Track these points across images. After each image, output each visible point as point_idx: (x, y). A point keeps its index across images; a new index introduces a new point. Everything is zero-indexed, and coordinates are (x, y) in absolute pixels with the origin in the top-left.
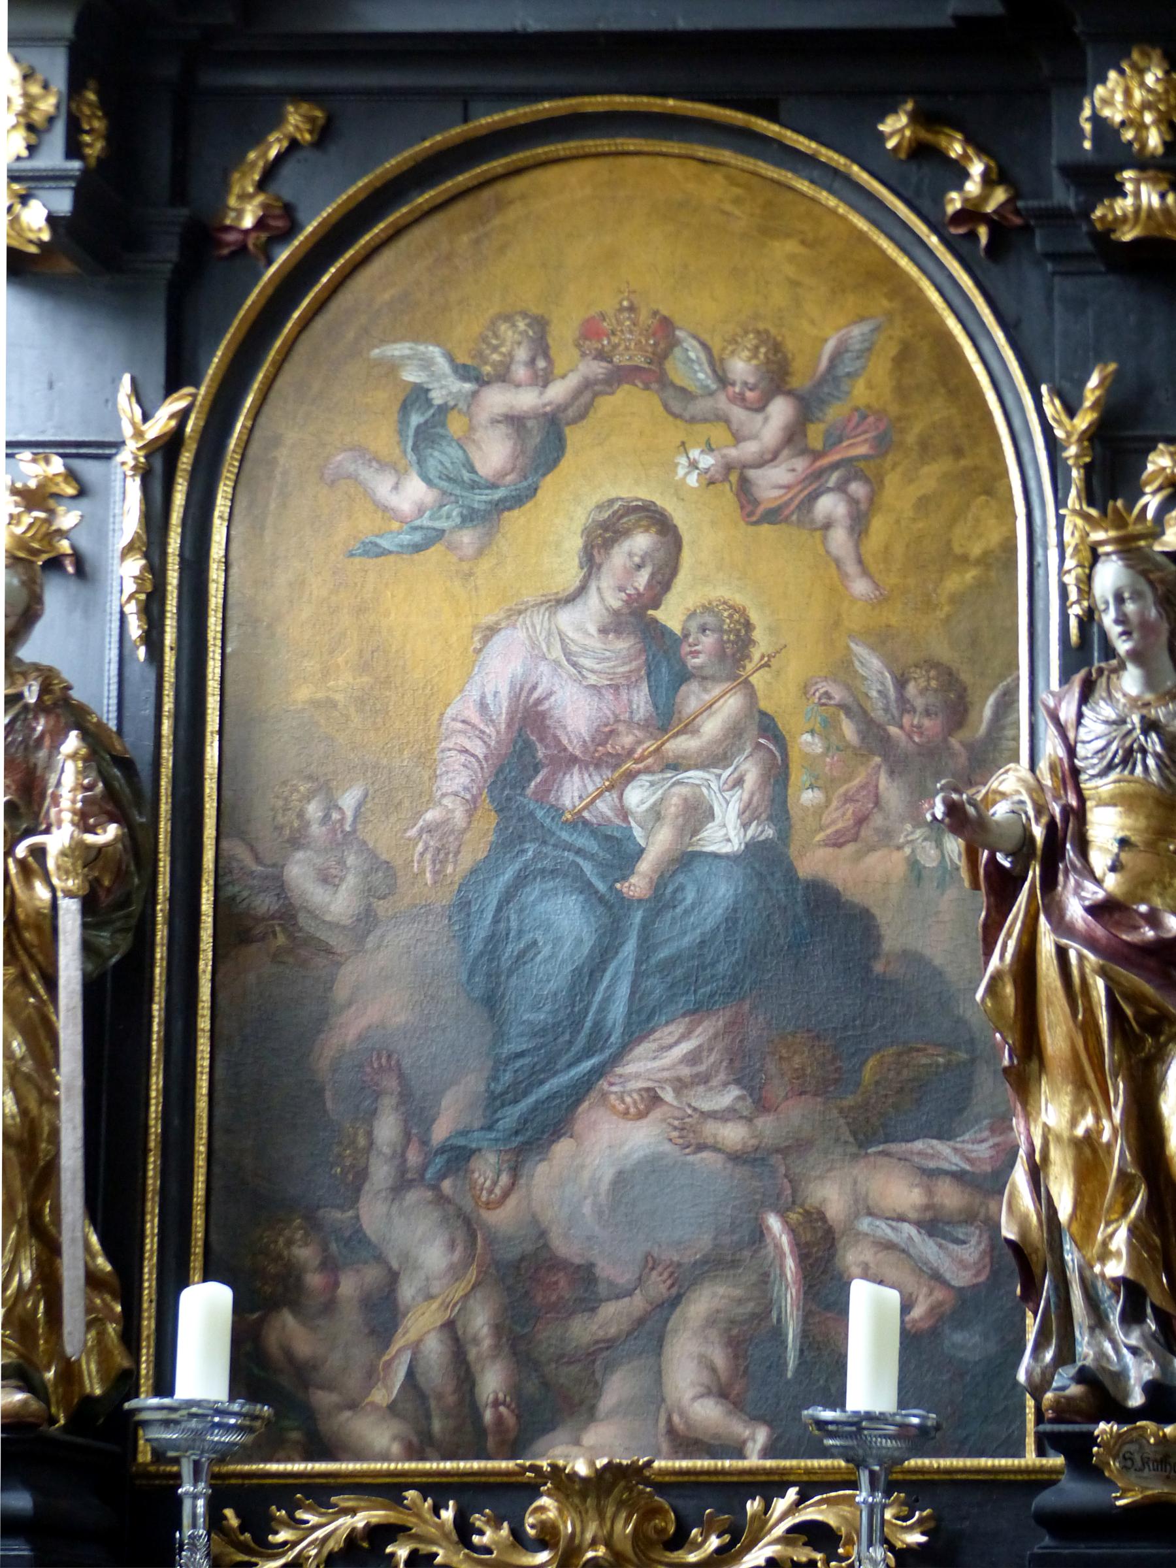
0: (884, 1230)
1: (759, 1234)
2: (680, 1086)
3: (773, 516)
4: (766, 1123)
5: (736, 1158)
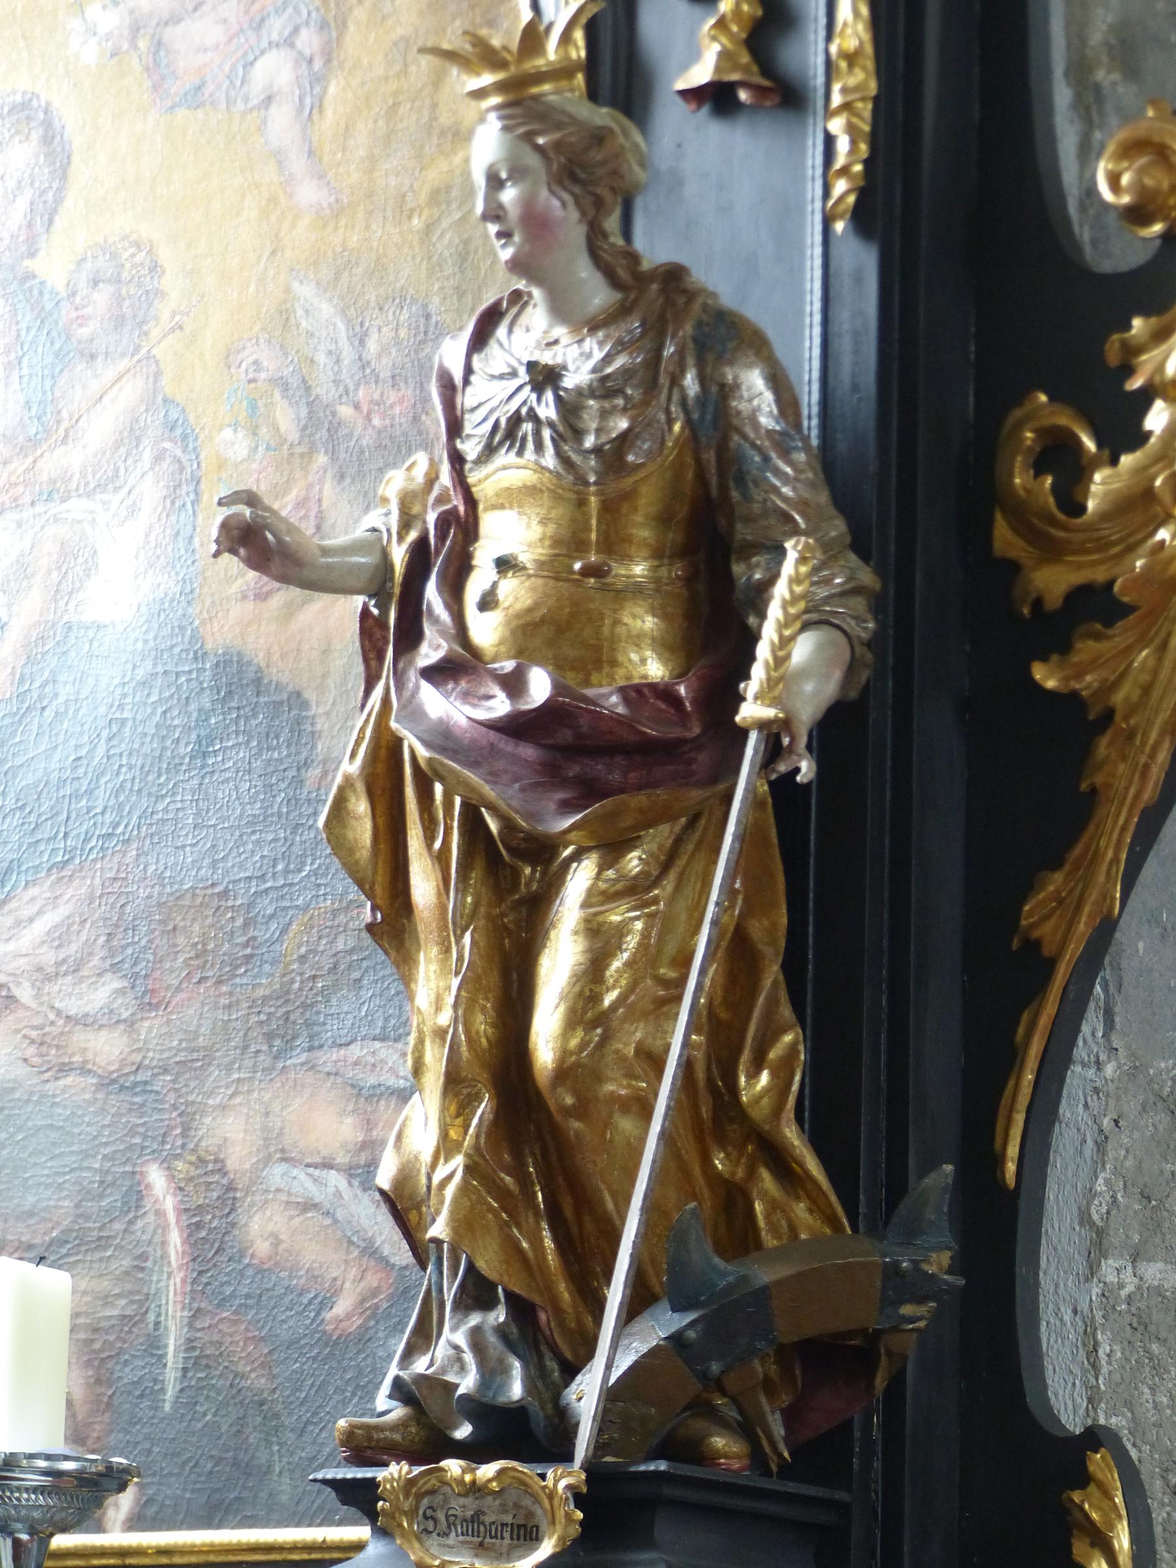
0: (303, 1183)
1: (136, 1195)
2: (44, 976)
3: (195, 97)
4: (151, 1026)
5: (111, 1083)
